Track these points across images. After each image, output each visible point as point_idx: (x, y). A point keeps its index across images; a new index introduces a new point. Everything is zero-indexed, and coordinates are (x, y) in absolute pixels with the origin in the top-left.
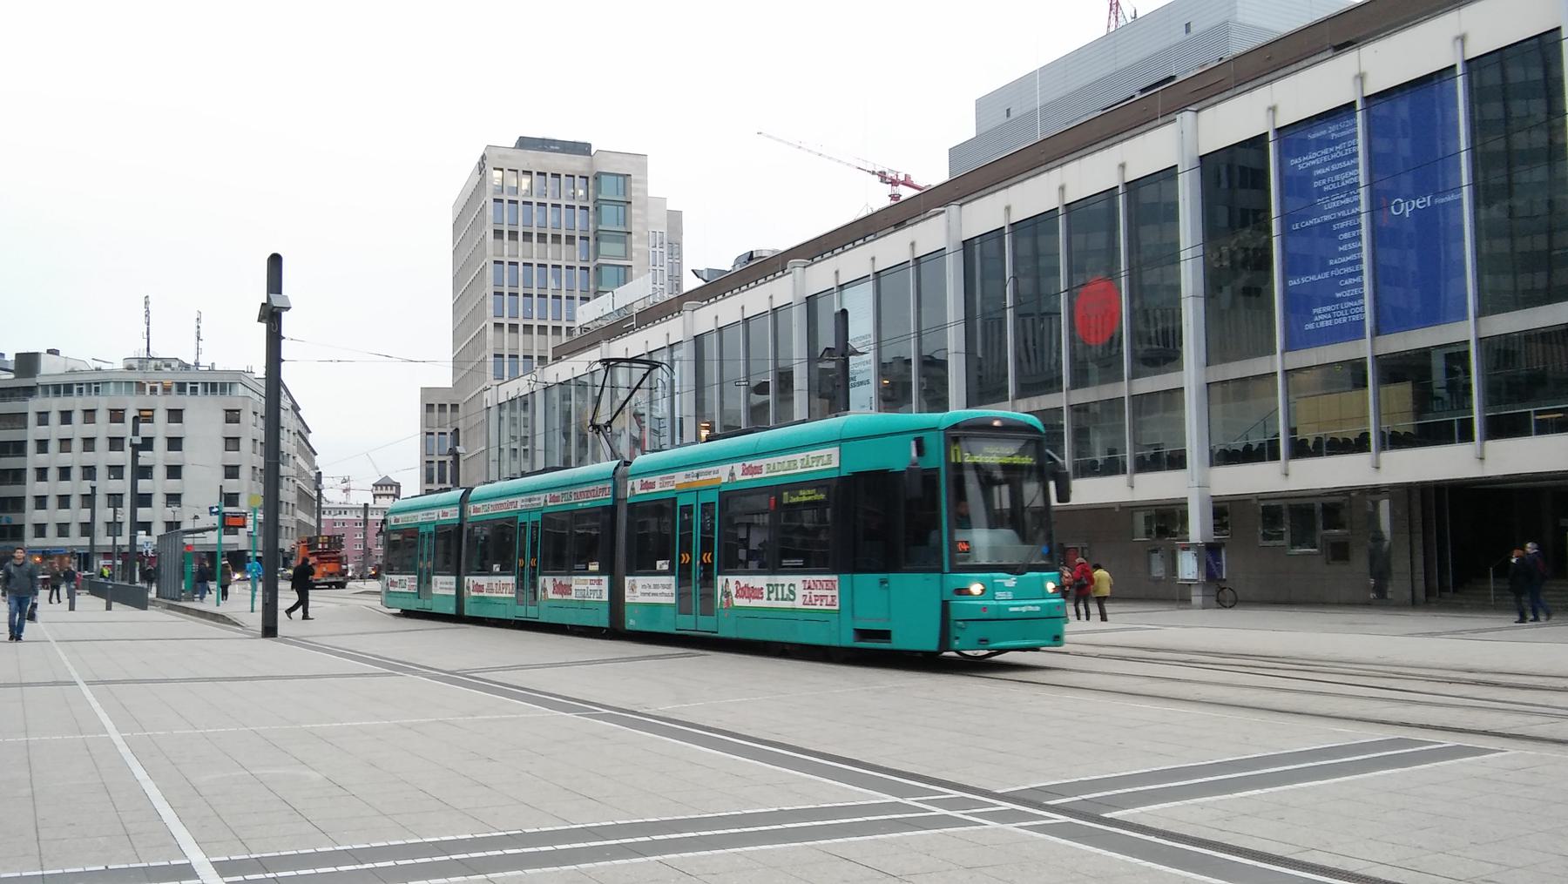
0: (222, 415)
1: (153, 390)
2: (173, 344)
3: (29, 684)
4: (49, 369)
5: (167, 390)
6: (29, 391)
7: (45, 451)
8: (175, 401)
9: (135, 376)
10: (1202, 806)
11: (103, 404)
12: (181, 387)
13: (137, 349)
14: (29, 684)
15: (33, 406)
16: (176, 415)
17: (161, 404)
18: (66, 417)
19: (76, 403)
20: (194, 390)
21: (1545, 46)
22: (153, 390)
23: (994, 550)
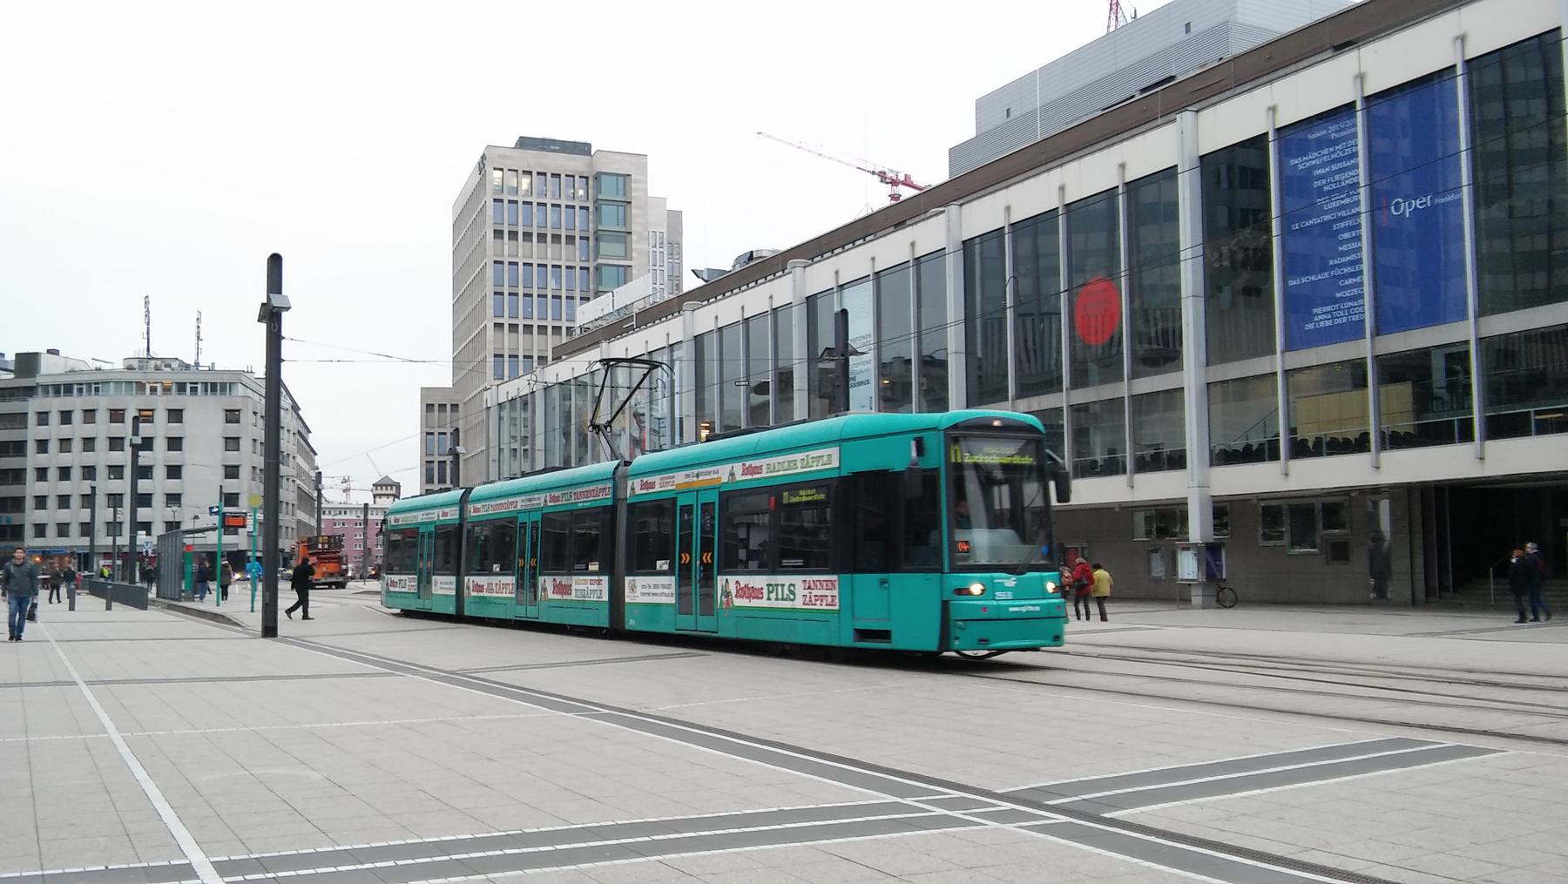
0: (222, 415)
1: (153, 390)
2: (173, 344)
3: (29, 684)
4: (49, 369)
5: (167, 390)
6: (29, 391)
7: (45, 451)
8: (175, 401)
9: (135, 376)
10: (1202, 806)
11: (103, 404)
12: (181, 387)
13: (137, 349)
14: (29, 684)
15: (33, 406)
16: (176, 415)
17: (161, 404)
18: (66, 417)
19: (76, 403)
20: (194, 390)
21: (1545, 46)
22: (153, 390)
23: (994, 550)
